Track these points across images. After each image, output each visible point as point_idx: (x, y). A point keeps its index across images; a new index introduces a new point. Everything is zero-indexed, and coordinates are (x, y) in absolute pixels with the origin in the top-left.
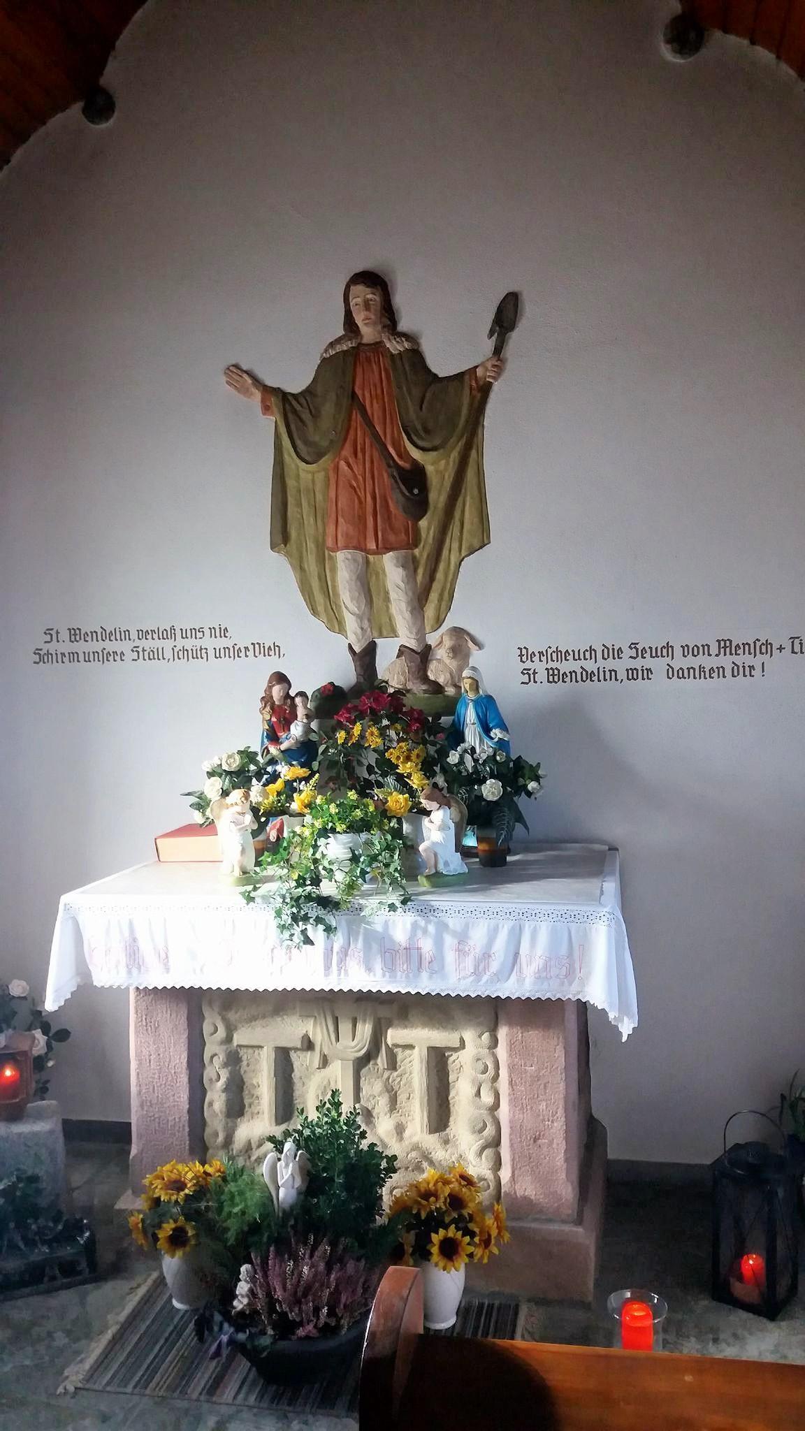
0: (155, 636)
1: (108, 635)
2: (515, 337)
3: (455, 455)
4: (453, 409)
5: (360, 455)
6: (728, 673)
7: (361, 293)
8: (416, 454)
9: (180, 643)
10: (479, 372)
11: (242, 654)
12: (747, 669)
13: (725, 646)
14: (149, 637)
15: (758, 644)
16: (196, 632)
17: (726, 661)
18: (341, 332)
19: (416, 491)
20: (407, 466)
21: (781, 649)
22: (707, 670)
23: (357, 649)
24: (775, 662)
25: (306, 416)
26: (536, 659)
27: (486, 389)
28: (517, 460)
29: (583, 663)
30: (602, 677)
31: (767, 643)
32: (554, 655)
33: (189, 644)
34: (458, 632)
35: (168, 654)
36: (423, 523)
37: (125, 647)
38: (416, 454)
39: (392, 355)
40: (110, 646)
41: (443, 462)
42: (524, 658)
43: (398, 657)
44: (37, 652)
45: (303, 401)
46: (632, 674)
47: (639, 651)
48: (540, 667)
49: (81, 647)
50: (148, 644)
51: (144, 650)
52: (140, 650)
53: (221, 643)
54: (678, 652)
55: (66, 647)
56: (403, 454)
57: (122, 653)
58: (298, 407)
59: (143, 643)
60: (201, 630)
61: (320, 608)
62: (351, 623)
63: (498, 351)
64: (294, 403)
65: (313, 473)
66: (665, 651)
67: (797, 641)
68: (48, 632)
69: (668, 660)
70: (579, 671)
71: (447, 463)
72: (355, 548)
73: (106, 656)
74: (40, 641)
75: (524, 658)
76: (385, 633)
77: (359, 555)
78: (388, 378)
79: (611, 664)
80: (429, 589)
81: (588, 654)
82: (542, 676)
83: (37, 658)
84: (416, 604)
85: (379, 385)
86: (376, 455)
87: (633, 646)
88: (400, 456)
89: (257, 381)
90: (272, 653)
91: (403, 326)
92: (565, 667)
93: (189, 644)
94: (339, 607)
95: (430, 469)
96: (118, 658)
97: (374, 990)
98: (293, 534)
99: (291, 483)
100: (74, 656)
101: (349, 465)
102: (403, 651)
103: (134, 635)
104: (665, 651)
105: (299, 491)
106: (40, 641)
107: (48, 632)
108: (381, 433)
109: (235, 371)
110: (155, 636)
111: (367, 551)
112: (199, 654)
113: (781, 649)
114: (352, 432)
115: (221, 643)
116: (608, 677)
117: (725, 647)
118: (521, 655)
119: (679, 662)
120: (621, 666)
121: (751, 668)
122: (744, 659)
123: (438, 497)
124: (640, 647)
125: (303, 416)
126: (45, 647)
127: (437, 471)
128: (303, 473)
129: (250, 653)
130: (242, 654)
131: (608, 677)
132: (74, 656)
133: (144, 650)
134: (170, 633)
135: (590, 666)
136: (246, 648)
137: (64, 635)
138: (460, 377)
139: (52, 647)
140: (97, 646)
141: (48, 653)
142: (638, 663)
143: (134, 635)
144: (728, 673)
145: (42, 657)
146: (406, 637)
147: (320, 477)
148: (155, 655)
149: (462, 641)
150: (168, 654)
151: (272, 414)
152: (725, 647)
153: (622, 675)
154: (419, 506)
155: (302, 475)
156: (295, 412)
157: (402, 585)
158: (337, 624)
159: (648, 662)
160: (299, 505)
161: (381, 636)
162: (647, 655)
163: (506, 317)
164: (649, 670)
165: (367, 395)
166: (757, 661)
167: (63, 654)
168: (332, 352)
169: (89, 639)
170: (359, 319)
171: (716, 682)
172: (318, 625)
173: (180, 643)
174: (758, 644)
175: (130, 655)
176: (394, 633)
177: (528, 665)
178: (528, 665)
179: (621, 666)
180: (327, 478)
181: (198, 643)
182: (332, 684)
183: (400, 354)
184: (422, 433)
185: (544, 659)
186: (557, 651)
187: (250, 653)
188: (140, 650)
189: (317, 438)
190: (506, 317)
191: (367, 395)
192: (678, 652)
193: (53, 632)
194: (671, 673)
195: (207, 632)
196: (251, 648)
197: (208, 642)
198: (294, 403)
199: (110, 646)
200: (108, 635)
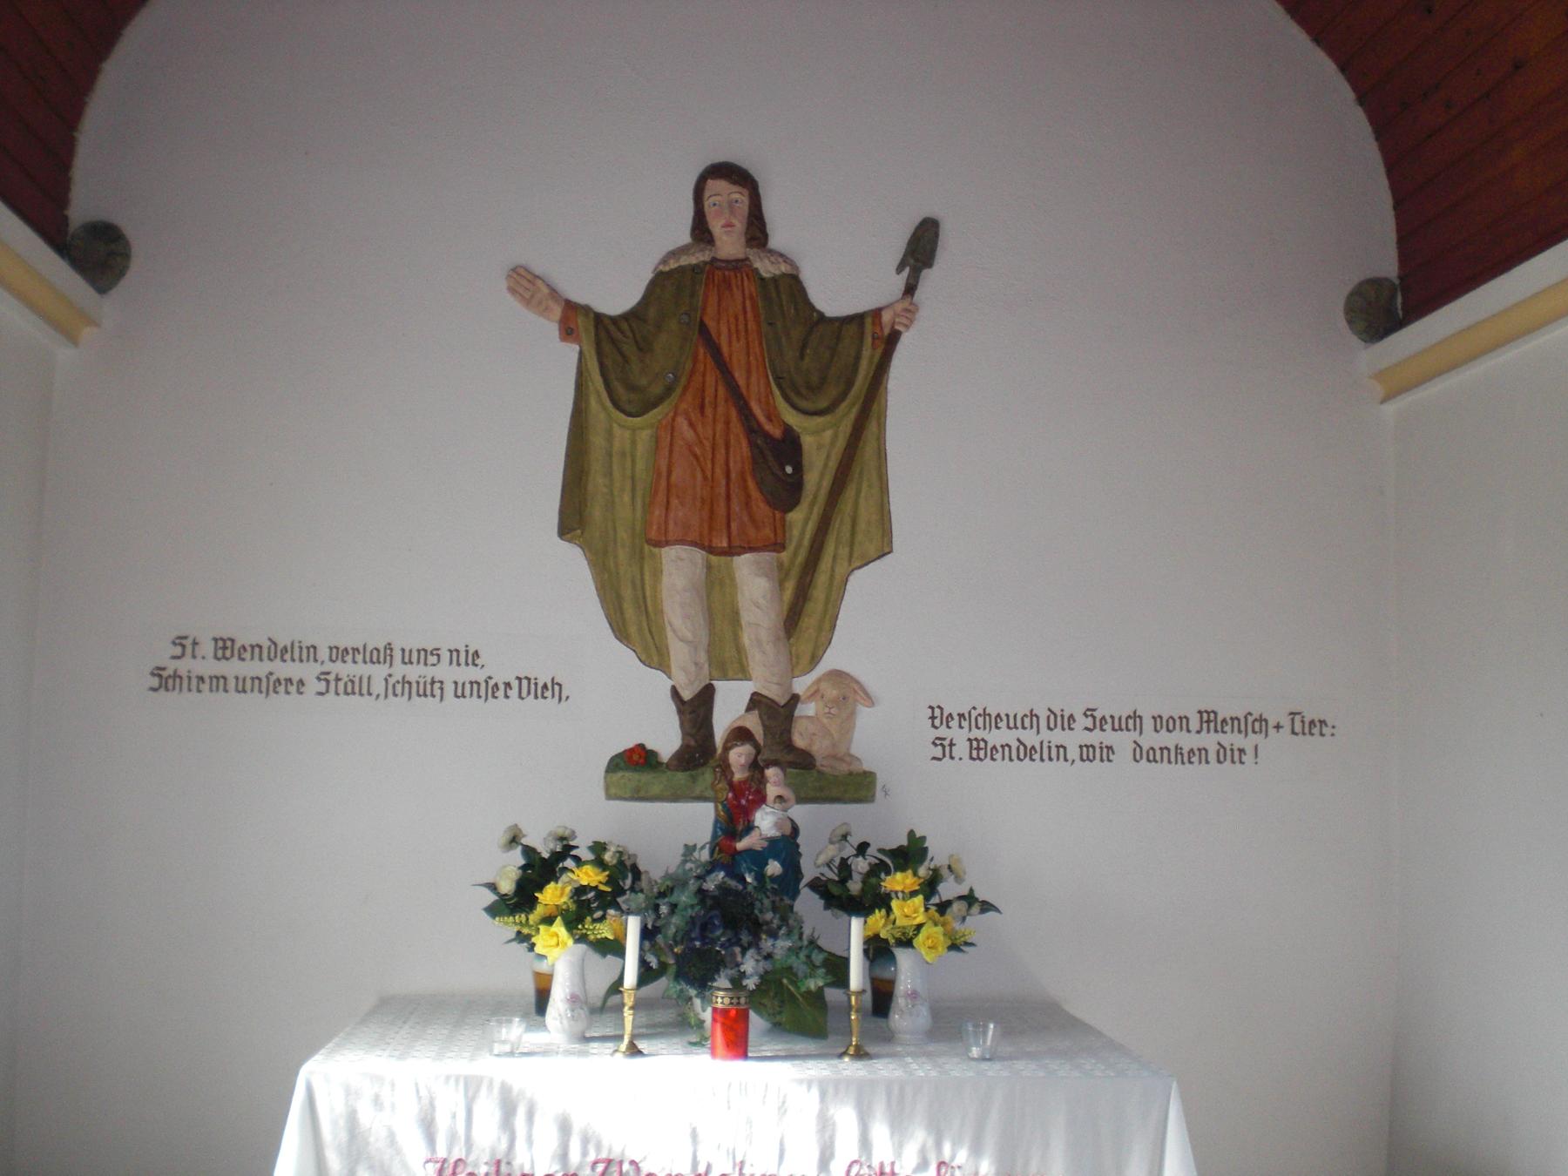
0: (359, 658)
1: (282, 652)
2: (931, 279)
3: (846, 427)
4: (847, 360)
5: (709, 411)
6: (1212, 757)
7: (719, 190)
8: (792, 418)
9: (399, 670)
10: (886, 317)
11: (500, 693)
12: (1236, 753)
13: (1209, 719)
14: (349, 658)
15: (1250, 719)
16: (427, 655)
17: (1209, 740)
18: (685, 237)
19: (789, 470)
20: (777, 432)
21: (1278, 727)
22: (1185, 752)
23: (687, 695)
24: (1277, 745)
25: (629, 349)
26: (954, 724)
27: (893, 339)
28: (934, 428)
29: (1020, 733)
30: (1045, 756)
31: (1261, 719)
32: (981, 720)
33: (414, 672)
34: (837, 676)
35: (378, 687)
36: (796, 516)
37: (308, 671)
38: (792, 418)
39: (763, 279)
40: (284, 670)
41: (828, 433)
42: (937, 722)
43: (748, 709)
44: (157, 672)
45: (625, 326)
46: (1088, 753)
47: (1099, 723)
48: (960, 736)
49: (232, 668)
50: (345, 669)
51: (338, 679)
52: (331, 677)
53: (468, 674)
54: (1148, 724)
55: (209, 667)
56: (772, 415)
57: (301, 682)
58: (618, 335)
59: (338, 668)
60: (436, 652)
61: (633, 630)
62: (679, 653)
63: (910, 290)
64: (612, 328)
65: (634, 430)
66: (1131, 722)
67: (1298, 718)
68: (179, 641)
69: (1134, 735)
70: (1014, 744)
71: (835, 436)
72: (694, 544)
73: (275, 685)
74: (163, 654)
75: (937, 722)
76: (730, 674)
77: (699, 555)
78: (754, 307)
79: (1058, 736)
80: (805, 613)
81: (1027, 721)
82: (961, 749)
83: (155, 682)
84: (782, 634)
85: (741, 318)
86: (722, 392)
87: (1089, 712)
88: (769, 419)
89: (554, 293)
90: (548, 694)
91: (775, 242)
92: (996, 737)
93: (414, 672)
94: (662, 629)
95: (807, 441)
96: (293, 689)
97: (801, 850)
98: (596, 512)
99: (597, 440)
100: (219, 682)
101: (691, 425)
102: (756, 702)
103: (323, 654)
104: (1131, 722)
105: (610, 455)
106: (163, 654)
107: (179, 641)
108: (742, 382)
109: (526, 284)
110: (359, 658)
111: (711, 550)
112: (429, 690)
113: (1278, 727)
114: (698, 378)
115: (468, 674)
116: (1054, 755)
117: (1208, 722)
118: (933, 718)
119: (1150, 739)
120: (1073, 740)
121: (1241, 751)
122: (1232, 739)
123: (816, 477)
124: (1098, 715)
125: (625, 348)
126: (172, 666)
127: (820, 447)
128: (630, 439)
129: (514, 693)
130: (500, 693)
131: (1054, 755)
132: (219, 682)
133: (338, 679)
134: (383, 655)
135: (1030, 738)
136: (508, 685)
137: (207, 648)
138: (858, 319)
139: (183, 666)
140: (260, 668)
141: (176, 676)
142: (1095, 738)
143: (323, 654)
144: (1212, 757)
145: (165, 680)
146: (763, 678)
147: (645, 436)
148: (355, 688)
149: (847, 692)
150: (378, 687)
151: (577, 340)
152: (1208, 722)
153: (1073, 753)
154: (788, 493)
155: (617, 430)
156: (613, 341)
157: (762, 601)
158: (655, 655)
159: (1109, 737)
160: (609, 474)
161: (725, 678)
162: (1108, 727)
163: (922, 248)
164: (1109, 748)
165: (724, 329)
166: (1247, 742)
167: (201, 679)
168: (673, 265)
169: (247, 655)
170: (716, 226)
171: (1196, 770)
172: (625, 656)
173: (399, 670)
174: (1250, 719)
175: (314, 686)
176: (743, 674)
177: (942, 732)
178: (942, 732)
179: (1073, 740)
180: (657, 440)
181: (430, 672)
182: (641, 747)
183: (775, 280)
184: (797, 391)
185: (965, 724)
186: (985, 714)
187: (514, 693)
188: (331, 677)
189: (644, 382)
190: (922, 248)
191: (724, 329)
192: (1148, 724)
193: (188, 643)
194: (1139, 753)
195: (445, 656)
196: (515, 684)
197: (446, 672)
198: (612, 328)
199: (284, 670)
200: (282, 652)
